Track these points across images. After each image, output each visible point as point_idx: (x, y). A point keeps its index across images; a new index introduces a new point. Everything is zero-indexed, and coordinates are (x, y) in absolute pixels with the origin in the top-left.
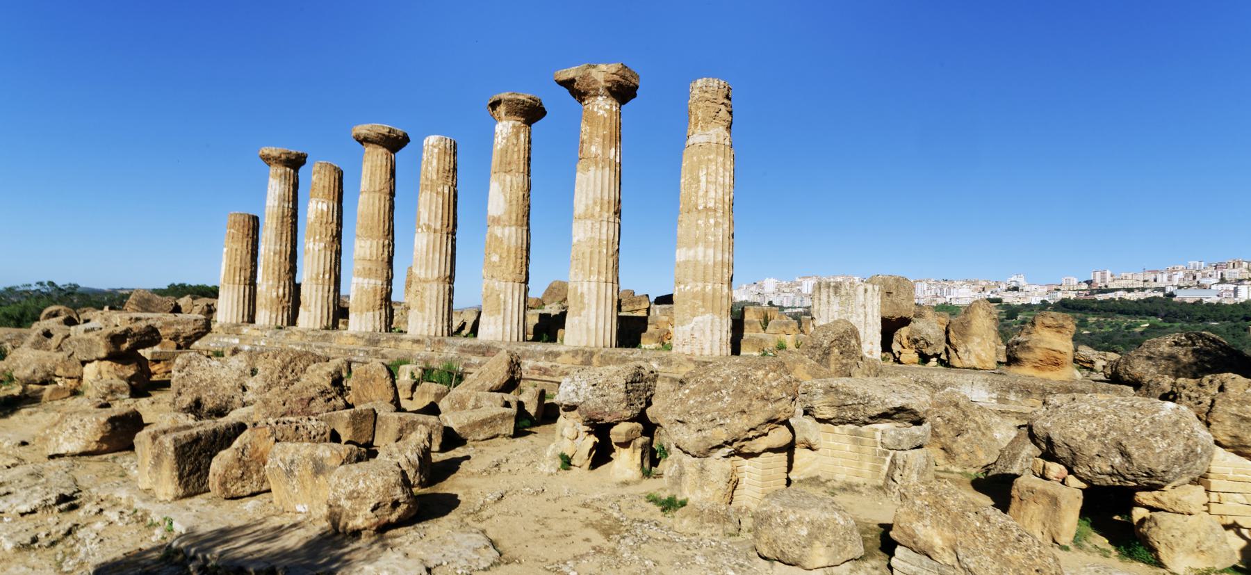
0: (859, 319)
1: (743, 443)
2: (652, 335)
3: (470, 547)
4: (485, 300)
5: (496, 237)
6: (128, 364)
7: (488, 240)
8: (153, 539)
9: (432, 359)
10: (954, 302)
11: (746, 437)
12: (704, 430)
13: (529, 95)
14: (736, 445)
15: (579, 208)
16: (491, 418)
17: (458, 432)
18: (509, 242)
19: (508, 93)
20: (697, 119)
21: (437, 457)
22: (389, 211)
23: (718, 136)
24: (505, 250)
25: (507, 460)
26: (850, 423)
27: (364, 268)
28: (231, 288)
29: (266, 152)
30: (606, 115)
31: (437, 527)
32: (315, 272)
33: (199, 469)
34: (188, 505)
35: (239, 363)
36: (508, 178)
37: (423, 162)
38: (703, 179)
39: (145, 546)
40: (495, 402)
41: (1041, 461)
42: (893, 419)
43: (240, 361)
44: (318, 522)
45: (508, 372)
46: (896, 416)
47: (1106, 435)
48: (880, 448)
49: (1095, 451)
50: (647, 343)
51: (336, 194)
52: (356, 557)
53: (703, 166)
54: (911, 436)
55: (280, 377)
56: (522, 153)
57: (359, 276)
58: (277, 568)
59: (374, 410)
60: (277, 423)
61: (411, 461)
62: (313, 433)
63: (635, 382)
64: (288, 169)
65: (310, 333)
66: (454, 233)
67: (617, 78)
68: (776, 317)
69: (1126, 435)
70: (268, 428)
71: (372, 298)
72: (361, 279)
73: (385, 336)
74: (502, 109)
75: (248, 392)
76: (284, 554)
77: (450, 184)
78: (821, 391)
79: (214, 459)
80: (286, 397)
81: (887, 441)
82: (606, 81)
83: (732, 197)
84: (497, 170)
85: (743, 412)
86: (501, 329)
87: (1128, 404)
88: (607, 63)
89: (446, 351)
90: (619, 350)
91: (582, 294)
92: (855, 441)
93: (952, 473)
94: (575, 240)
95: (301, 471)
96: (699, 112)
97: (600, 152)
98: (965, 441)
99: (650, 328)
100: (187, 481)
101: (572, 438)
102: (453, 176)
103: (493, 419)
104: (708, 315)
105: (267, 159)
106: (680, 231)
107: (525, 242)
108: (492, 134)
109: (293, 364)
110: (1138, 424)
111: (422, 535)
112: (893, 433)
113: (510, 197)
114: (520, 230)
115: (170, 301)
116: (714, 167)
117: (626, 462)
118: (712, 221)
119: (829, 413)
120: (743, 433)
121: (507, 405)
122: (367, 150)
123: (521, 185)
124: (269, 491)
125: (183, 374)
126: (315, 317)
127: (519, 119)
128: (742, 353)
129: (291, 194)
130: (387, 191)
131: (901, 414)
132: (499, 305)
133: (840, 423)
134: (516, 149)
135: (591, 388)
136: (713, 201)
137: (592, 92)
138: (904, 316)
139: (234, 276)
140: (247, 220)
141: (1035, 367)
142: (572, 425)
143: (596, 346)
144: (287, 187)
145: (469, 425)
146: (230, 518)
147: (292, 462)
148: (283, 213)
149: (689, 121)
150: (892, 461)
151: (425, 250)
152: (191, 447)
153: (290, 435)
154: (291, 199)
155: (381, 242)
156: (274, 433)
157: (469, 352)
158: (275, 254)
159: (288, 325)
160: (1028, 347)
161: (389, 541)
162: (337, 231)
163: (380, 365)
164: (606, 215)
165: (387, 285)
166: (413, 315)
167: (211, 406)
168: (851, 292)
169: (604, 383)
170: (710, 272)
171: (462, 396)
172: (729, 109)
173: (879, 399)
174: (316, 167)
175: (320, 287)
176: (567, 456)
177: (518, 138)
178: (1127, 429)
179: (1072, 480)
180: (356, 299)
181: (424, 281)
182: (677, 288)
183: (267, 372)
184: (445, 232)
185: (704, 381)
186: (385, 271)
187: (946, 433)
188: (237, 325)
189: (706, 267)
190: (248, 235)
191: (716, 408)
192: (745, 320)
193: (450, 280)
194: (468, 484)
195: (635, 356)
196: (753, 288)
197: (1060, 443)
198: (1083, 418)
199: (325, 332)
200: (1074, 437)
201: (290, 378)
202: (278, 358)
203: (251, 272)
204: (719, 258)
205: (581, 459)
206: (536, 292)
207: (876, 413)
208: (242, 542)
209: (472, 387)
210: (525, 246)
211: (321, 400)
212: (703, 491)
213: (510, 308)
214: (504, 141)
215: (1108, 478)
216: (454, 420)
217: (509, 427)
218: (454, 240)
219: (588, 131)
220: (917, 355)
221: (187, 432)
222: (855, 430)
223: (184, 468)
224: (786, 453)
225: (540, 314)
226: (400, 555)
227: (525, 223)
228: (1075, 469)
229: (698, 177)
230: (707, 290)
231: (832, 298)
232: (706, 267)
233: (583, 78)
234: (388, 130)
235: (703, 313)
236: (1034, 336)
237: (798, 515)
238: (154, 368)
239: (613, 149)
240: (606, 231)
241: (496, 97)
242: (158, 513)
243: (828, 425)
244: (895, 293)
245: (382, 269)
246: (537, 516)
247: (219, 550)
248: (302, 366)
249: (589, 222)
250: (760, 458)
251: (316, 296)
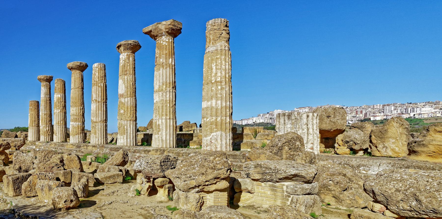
0: (303, 132)
1: (204, 187)
2: (195, 142)
3: (95, 217)
4: (119, 129)
5: (122, 103)
6: (2, 155)
7: (119, 104)
8: (8, 207)
9: (100, 153)
10: (417, 116)
11: (205, 184)
12: (187, 181)
13: (133, 41)
14: (200, 187)
15: (156, 87)
16: (113, 175)
17: (101, 180)
18: (128, 104)
19: (124, 41)
20: (210, 39)
21: (91, 189)
22: (82, 95)
23: (221, 46)
24: (126, 108)
25: (117, 191)
26: (269, 181)
27: (74, 118)
28: (32, 129)
29: (40, 77)
30: (166, 44)
31: (86, 210)
32: (58, 121)
33: (19, 188)
34: (17, 198)
35: (31, 154)
36: (126, 77)
37: (93, 74)
38: (214, 68)
39: (6, 209)
40: (116, 170)
41: (372, 203)
42: (293, 180)
43: (32, 154)
44: (51, 206)
45: (122, 158)
46: (293, 179)
47: (407, 190)
48: (286, 194)
49: (400, 198)
50: (192, 146)
51: (63, 90)
52: (59, 216)
53: (214, 62)
54: (303, 189)
55: (44, 160)
56: (131, 66)
57: (72, 121)
58: (37, 217)
59: (71, 171)
60: (40, 174)
61: (80, 188)
62: (50, 178)
63: (165, 162)
64: (47, 83)
65: (57, 144)
66: (106, 102)
67: (171, 26)
68: (262, 132)
69: (420, 190)
70: (37, 175)
71: (77, 130)
72: (73, 123)
73: (83, 144)
74: (122, 48)
75: (35, 165)
76: (40, 213)
77: (104, 82)
78: (253, 166)
79: (23, 184)
80: (45, 166)
81: (289, 190)
82: (166, 29)
83: (230, 74)
84: (121, 75)
85: (203, 174)
86: (126, 141)
87: (427, 174)
88: (166, 20)
89: (105, 150)
90: (176, 149)
91: (159, 125)
92: (272, 190)
93: (340, 209)
94: (155, 101)
95: (46, 189)
96: (210, 35)
97: (164, 61)
98: (350, 194)
99: (195, 139)
100: (16, 191)
101: (140, 183)
102: (105, 79)
103: (114, 176)
104: (219, 132)
105: (40, 80)
106: (204, 93)
107: (134, 104)
108: (119, 59)
109: (48, 154)
110: (429, 185)
111: (81, 212)
112: (292, 187)
113: (127, 85)
114: (132, 99)
115: (14, 133)
116: (220, 61)
117: (162, 194)
118: (219, 87)
119: (257, 177)
120: (203, 183)
121: (121, 171)
122: (73, 72)
123: (131, 80)
124: (38, 196)
125: (16, 158)
126: (59, 138)
127: (129, 51)
128: (241, 150)
129: (49, 92)
130: (81, 87)
131: (297, 178)
132: (124, 131)
133: (265, 182)
134: (129, 65)
135: (146, 164)
136: (220, 78)
137: (160, 35)
138: (339, 128)
139: (33, 124)
140: (35, 103)
141: (429, 156)
142: (140, 178)
143: (166, 147)
144: (47, 89)
145: (105, 178)
146: (27, 203)
147: (43, 186)
148: (46, 99)
149: (206, 41)
150: (291, 200)
151: (95, 109)
152: (17, 180)
153: (43, 178)
154: (48, 94)
155: (80, 108)
156: (39, 177)
157: (114, 151)
158: (44, 115)
159: (50, 141)
160: (423, 144)
161: (70, 213)
162: (64, 104)
163: (75, 155)
164: (168, 89)
165: (83, 124)
166: (92, 136)
167: (24, 169)
168: (298, 118)
169: (151, 162)
170: (220, 112)
171: (103, 167)
172: (228, 32)
173: (283, 170)
174: (56, 81)
175: (60, 126)
176: (139, 190)
177: (129, 60)
178: (421, 187)
179: (388, 213)
180: (72, 130)
181: (96, 122)
182: (203, 120)
183: (40, 158)
184: (102, 102)
185: (189, 161)
186: (82, 119)
187: (335, 189)
188: (34, 141)
189: (217, 109)
190: (36, 108)
191: (192, 172)
192: (244, 133)
193: (106, 121)
194: (101, 198)
195: (184, 151)
196: (267, 116)
197: (379, 194)
198: (394, 181)
199: (62, 143)
200: (387, 190)
201: (47, 160)
202: (43, 153)
203: (38, 122)
204: (224, 104)
205: (144, 191)
206: (141, 124)
207: (281, 177)
208: (29, 209)
209: (108, 164)
210: (134, 105)
211: (56, 167)
212: (187, 205)
213: (129, 132)
214: (123, 62)
215: (410, 213)
216: (99, 176)
217: (121, 179)
218: (106, 105)
219: (159, 52)
220: (348, 149)
221: (15, 176)
222: (273, 185)
223: (15, 187)
224: (227, 192)
225: (144, 134)
226: (72, 217)
227: (134, 95)
228: (389, 207)
229: (212, 67)
230: (218, 120)
231: (287, 121)
232: (217, 109)
233: (155, 29)
234: (80, 63)
235: (216, 131)
236: (428, 138)
237: (215, 215)
238: (9, 157)
239: (171, 59)
240: (169, 96)
241: (119, 44)
242: (9, 200)
243: (258, 182)
244: (332, 116)
245: (80, 118)
246: (122, 210)
247: (23, 210)
248: (50, 156)
249: (161, 93)
250: (213, 194)
251: (59, 130)
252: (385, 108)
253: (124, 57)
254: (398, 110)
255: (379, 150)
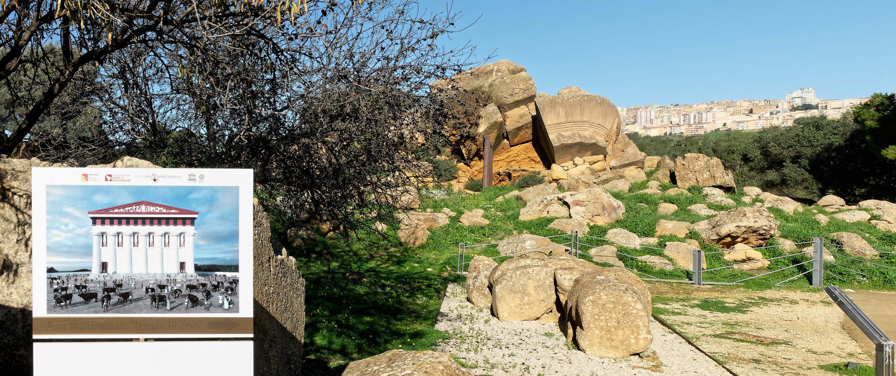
252: (639, 113)
253: (185, 70)
254: (664, 119)
255: (533, 162)
